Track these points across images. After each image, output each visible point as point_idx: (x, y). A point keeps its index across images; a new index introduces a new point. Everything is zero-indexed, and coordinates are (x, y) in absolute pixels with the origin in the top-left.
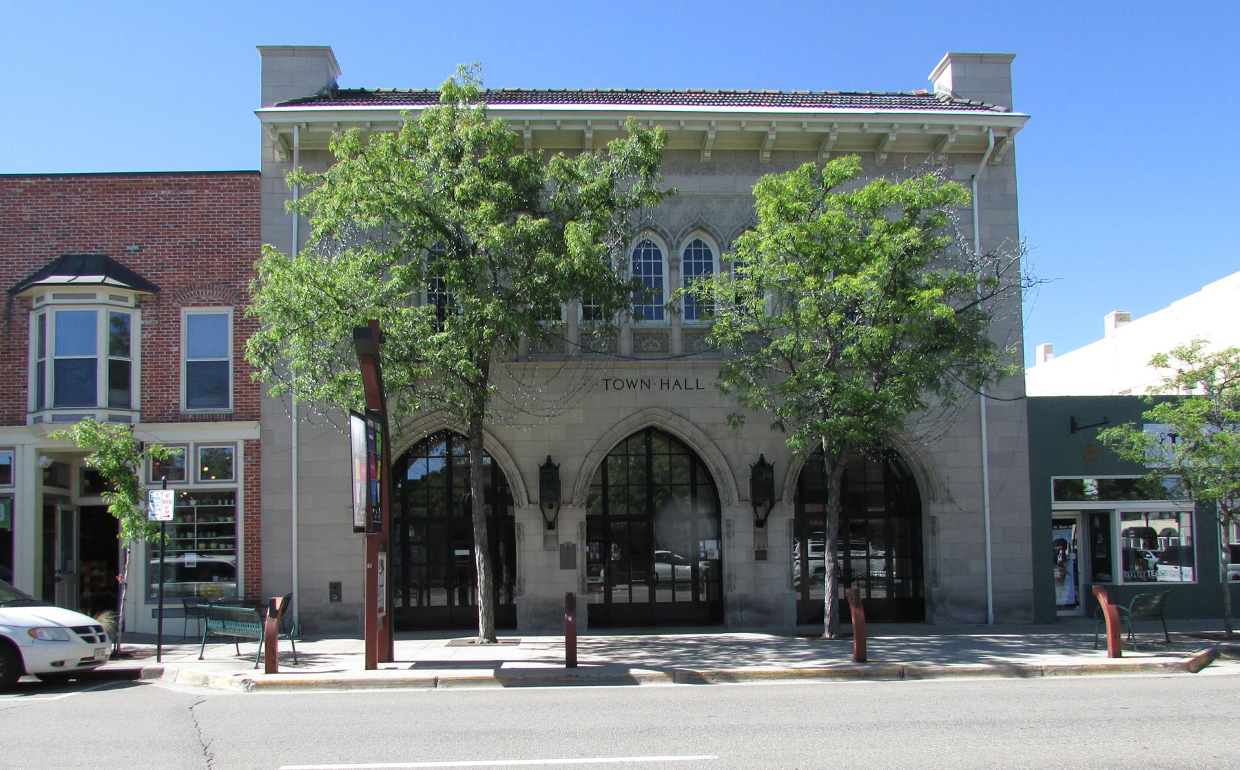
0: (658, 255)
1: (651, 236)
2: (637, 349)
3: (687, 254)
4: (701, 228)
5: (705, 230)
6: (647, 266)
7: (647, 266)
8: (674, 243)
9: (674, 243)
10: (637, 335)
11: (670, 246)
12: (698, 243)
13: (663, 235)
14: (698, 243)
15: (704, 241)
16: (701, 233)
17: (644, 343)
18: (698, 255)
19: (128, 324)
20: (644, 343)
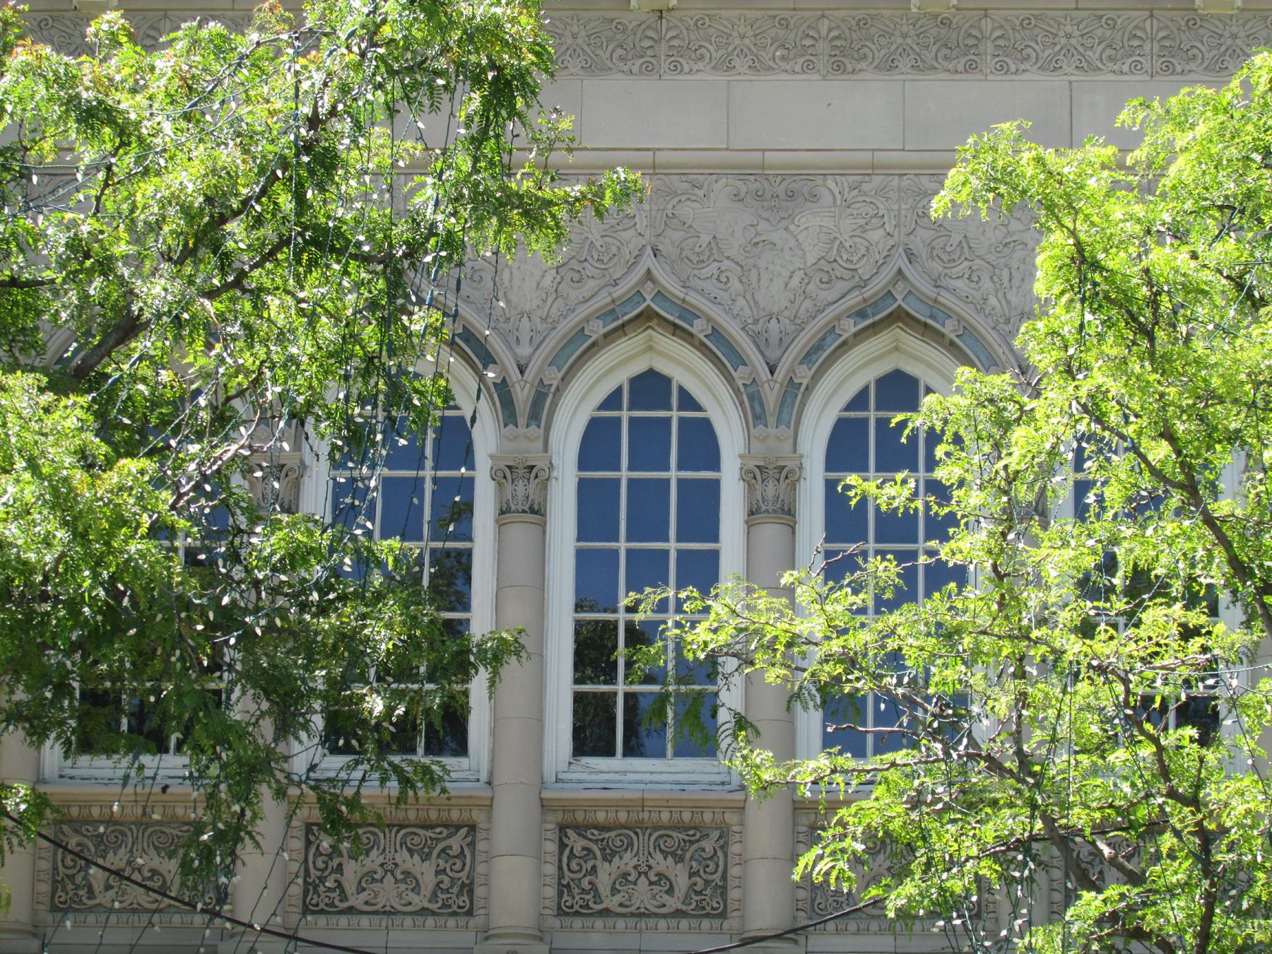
0: (701, 444)
1: (686, 368)
2: (572, 900)
3: (597, 443)
4: (900, 317)
5: (927, 331)
6: (648, 499)
7: (648, 499)
8: (771, 396)
9: (771, 396)
10: (579, 834)
11: (754, 408)
12: (651, 387)
13: (719, 350)
14: (651, 387)
15: (679, 377)
16: (912, 342)
17: (606, 874)
18: (649, 445)
19: (577, 732)
20: (606, 874)
